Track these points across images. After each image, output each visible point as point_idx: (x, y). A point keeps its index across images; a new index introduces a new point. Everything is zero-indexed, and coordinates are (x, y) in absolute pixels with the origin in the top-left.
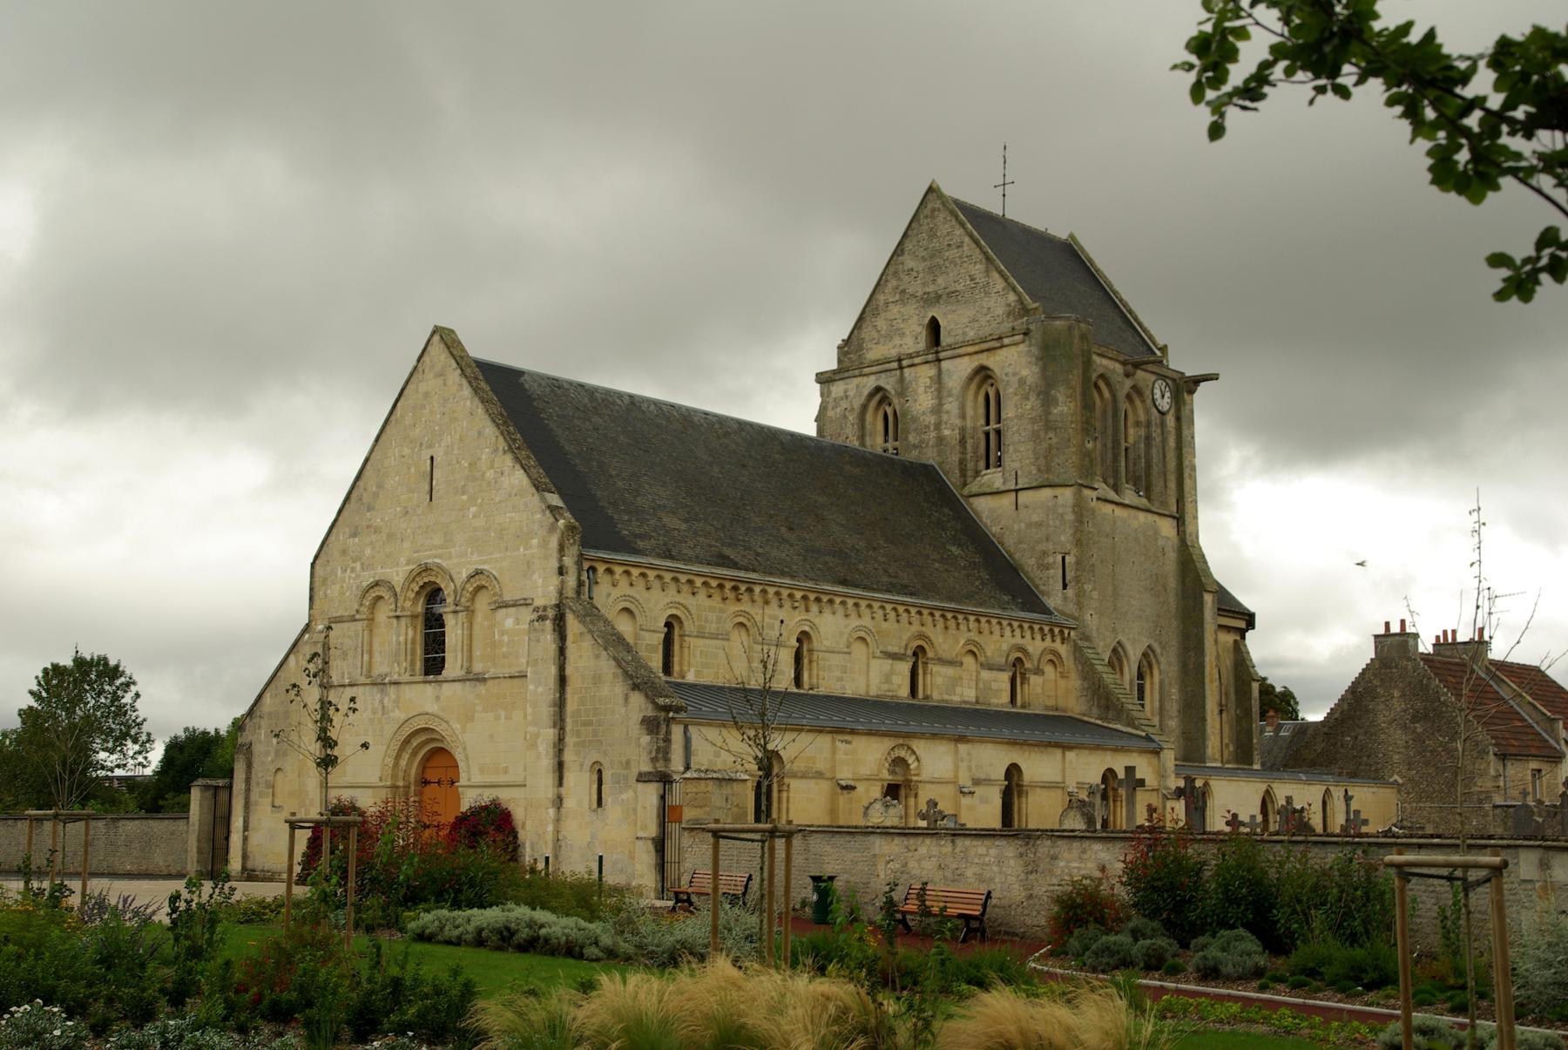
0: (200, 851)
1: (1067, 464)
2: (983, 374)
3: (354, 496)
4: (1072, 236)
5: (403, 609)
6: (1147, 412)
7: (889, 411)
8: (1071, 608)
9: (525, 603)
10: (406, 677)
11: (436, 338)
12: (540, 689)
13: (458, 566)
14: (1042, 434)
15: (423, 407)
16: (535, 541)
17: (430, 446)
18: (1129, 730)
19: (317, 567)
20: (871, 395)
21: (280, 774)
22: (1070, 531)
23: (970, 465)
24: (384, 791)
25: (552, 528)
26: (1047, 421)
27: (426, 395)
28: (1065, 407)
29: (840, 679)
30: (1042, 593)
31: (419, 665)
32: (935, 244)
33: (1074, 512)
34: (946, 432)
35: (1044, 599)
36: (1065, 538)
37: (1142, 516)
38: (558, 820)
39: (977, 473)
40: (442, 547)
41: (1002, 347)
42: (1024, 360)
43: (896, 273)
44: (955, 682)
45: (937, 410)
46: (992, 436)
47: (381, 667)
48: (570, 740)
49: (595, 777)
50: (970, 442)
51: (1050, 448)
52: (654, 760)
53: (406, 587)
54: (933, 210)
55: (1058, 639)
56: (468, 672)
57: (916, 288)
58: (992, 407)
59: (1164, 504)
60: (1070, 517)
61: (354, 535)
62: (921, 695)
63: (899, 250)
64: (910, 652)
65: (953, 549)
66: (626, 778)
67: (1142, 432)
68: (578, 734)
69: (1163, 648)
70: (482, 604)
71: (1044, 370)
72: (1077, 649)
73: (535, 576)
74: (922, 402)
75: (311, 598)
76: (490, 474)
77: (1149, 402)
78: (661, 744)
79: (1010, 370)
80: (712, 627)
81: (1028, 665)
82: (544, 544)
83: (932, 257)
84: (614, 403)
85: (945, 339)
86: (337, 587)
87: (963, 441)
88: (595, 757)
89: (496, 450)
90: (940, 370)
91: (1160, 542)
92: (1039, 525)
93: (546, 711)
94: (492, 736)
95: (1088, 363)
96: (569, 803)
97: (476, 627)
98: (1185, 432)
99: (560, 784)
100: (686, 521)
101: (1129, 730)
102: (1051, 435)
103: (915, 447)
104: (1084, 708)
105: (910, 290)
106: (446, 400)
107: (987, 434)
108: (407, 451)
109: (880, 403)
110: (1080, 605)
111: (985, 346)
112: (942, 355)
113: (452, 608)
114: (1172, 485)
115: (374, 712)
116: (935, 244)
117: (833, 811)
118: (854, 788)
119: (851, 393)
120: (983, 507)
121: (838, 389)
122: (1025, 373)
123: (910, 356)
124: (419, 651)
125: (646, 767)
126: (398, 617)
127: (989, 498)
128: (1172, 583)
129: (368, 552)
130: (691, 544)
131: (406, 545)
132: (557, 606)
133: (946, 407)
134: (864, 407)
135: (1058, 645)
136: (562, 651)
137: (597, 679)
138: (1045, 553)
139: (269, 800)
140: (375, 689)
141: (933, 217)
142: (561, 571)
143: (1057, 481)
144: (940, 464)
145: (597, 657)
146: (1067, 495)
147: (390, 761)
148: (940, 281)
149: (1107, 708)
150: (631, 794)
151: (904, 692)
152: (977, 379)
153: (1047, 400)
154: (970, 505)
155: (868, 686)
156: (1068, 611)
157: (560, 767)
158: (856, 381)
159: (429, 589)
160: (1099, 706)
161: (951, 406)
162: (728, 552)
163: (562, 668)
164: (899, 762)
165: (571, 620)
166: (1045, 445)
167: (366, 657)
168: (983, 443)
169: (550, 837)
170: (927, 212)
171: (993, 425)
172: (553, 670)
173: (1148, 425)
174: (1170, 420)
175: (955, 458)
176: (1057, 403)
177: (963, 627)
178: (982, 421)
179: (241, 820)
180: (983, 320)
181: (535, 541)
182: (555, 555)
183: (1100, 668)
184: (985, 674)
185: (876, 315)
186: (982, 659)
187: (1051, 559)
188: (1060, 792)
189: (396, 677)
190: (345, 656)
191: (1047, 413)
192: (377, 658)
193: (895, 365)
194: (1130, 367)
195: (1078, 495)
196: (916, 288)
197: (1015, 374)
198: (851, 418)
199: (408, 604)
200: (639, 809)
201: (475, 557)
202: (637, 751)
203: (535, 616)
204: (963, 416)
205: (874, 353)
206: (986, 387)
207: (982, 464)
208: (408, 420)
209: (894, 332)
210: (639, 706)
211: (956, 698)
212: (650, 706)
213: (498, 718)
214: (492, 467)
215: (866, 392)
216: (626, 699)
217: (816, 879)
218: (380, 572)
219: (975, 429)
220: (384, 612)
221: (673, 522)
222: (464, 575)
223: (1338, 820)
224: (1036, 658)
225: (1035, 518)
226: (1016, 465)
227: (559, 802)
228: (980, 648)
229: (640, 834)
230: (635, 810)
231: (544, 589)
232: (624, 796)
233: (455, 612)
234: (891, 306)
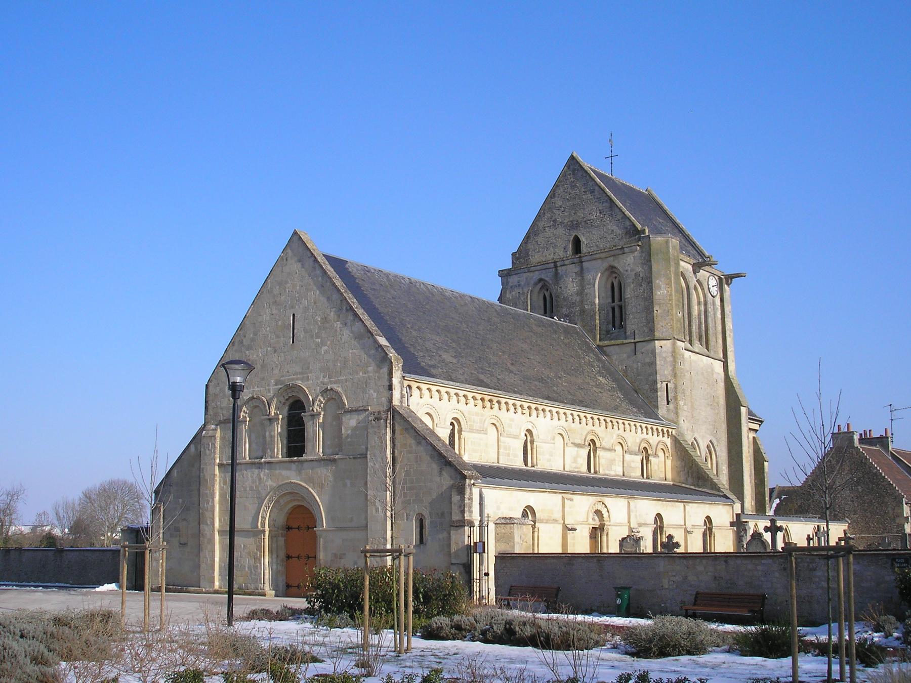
2: (612, 270)
7: (547, 294)
8: (672, 416)
15: (287, 282)
17: (292, 307)
19: (210, 388)
29: (549, 460)
44: (612, 462)
55: (666, 435)
60: (670, 359)
62: (592, 471)
64: (587, 444)
65: (601, 378)
69: (718, 441)
75: (206, 408)
80: (477, 426)
84: (400, 282)
89: (341, 309)
91: (715, 376)
95: (678, 265)
100: (455, 357)
104: (683, 479)
107: (613, 309)
110: (677, 413)
114: (720, 341)
117: (565, 543)
118: (575, 530)
119: (522, 283)
121: (513, 280)
128: (722, 401)
130: (461, 372)
151: (584, 468)
158: (525, 275)
159: (291, 401)
160: (693, 477)
162: (482, 377)
164: (598, 513)
168: (611, 314)
177: (616, 427)
178: (610, 300)
180: (609, 238)
181: (370, 369)
184: (627, 456)
185: (536, 235)
186: (625, 448)
193: (552, 265)
195: (674, 344)
205: (535, 258)
211: (612, 473)
221: (447, 357)
223: (780, 545)
229: (454, 561)
232: (441, 536)
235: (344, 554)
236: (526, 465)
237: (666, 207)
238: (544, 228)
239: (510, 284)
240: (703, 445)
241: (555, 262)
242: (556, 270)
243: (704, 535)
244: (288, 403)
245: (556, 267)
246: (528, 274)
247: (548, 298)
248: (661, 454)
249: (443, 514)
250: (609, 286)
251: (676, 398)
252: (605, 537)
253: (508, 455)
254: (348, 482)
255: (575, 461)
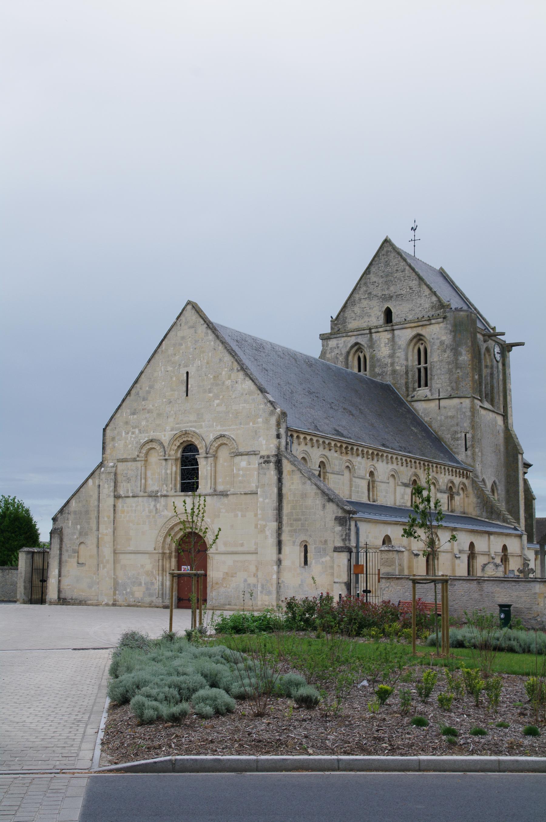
0: (25, 588)
1: (467, 386)
2: (419, 338)
3: (133, 392)
4: (441, 268)
5: (169, 456)
6: (491, 361)
8: (469, 461)
9: (255, 453)
10: (172, 493)
11: (189, 307)
12: (267, 501)
13: (206, 433)
14: (454, 370)
16: (260, 420)
17: (186, 366)
18: (505, 524)
19: (108, 431)
20: (352, 347)
21: (82, 546)
22: (468, 421)
23: (411, 385)
24: (157, 555)
25: (272, 413)
26: (457, 364)
27: (183, 338)
28: (465, 357)
29: (385, 497)
30: (455, 453)
31: (179, 486)
32: (389, 269)
33: (470, 411)
34: (398, 368)
35: (456, 456)
36: (466, 424)
37: (491, 414)
38: (278, 572)
39: (414, 390)
40: (196, 422)
41: (430, 324)
42: (443, 332)
43: (365, 284)
45: (392, 356)
46: (423, 371)
47: (153, 487)
48: (285, 528)
49: (303, 549)
50: (410, 374)
51: (458, 377)
52: (344, 540)
53: (171, 443)
54: (387, 252)
56: (215, 491)
57: (377, 291)
58: (422, 355)
59: (499, 408)
60: (469, 414)
61: (134, 414)
63: (367, 271)
64: (411, 483)
66: (324, 550)
67: (489, 371)
68: (291, 525)
69: (499, 482)
70: (223, 454)
71: (454, 337)
72: (474, 482)
73: (261, 439)
74: (383, 351)
76: (228, 383)
77: (492, 355)
78: (348, 532)
79: (435, 336)
81: (454, 490)
82: (267, 421)
83: (387, 276)
85: (395, 319)
86: (123, 442)
87: (407, 373)
88: (303, 537)
89: (232, 369)
90: (393, 334)
92: (452, 417)
93: (271, 513)
94: (232, 526)
96: (286, 563)
97: (219, 467)
98: (507, 372)
99: (280, 551)
101: (509, 526)
102: (459, 371)
103: (379, 375)
105: (374, 293)
106: (196, 341)
107: (419, 370)
108: (170, 369)
109: (356, 351)
110: (474, 459)
111: (421, 323)
112: (395, 327)
113: (205, 455)
114: (501, 399)
115: (150, 512)
116: (389, 269)
119: (341, 346)
120: (420, 407)
121: (332, 343)
122: (444, 338)
123: (377, 327)
124: (179, 478)
125: (339, 544)
126: (166, 460)
127: (423, 402)
128: (502, 449)
129: (144, 423)
131: (171, 420)
132: (277, 455)
133: (398, 354)
134: (348, 353)
135: (464, 480)
136: (280, 480)
137: (304, 496)
138: (456, 432)
139: (75, 560)
140: (150, 499)
141: (387, 255)
142: (278, 436)
143: (462, 395)
144: (394, 384)
145: (304, 483)
146: (467, 402)
147: (161, 539)
148: (392, 288)
149: (492, 513)
150: (328, 558)
152: (415, 340)
153: (456, 353)
154: (412, 406)
155: (395, 500)
156: (468, 463)
157: (280, 543)
158: (343, 339)
160: (487, 512)
161: (400, 354)
163: (280, 490)
165: (285, 462)
166: (455, 376)
167: (143, 481)
169: (274, 581)
170: (383, 252)
171: (423, 365)
172: (275, 490)
173: (492, 367)
174: (500, 365)
175: (403, 381)
176: (461, 354)
178: (416, 363)
179: (57, 572)
181: (260, 420)
182: (274, 428)
183: (487, 492)
185: (354, 304)
186: (437, 487)
187: (459, 435)
188: (487, 556)
189: (165, 493)
190: (128, 480)
191: (457, 359)
192: (150, 482)
193: (368, 331)
194: (487, 338)
195: (472, 402)
196: (377, 291)
197: (438, 339)
198: (341, 358)
199: (173, 452)
200: (335, 566)
201: (219, 428)
202: (334, 535)
203: (262, 460)
204: (407, 360)
205: (352, 325)
206: (419, 345)
207: (416, 385)
208: (171, 351)
209: (364, 314)
210: (332, 510)
212: (340, 511)
213: (236, 516)
214: (229, 378)
215: (349, 345)
216: (324, 506)
217: (501, 606)
218: (152, 435)
219: (413, 366)
220: (154, 458)
222: (212, 437)
224: (457, 486)
225: (450, 414)
226: (439, 386)
227: (279, 562)
228: (437, 481)
229: (336, 580)
230: (332, 567)
231: (267, 445)
233: (206, 457)
234: (363, 301)
235: (236, 573)
236: (369, 500)
237: (365, 268)
238: (360, 299)
239: (330, 346)
240: (489, 485)
241: (370, 329)
242: (371, 336)
243: (469, 557)
244: (182, 447)
245: (371, 333)
246: (346, 338)
247: (362, 360)
248: (461, 492)
249: (326, 541)
250: (416, 351)
251: (473, 446)
252: (436, 561)
253: (358, 492)
254: (240, 514)
255: (403, 498)
